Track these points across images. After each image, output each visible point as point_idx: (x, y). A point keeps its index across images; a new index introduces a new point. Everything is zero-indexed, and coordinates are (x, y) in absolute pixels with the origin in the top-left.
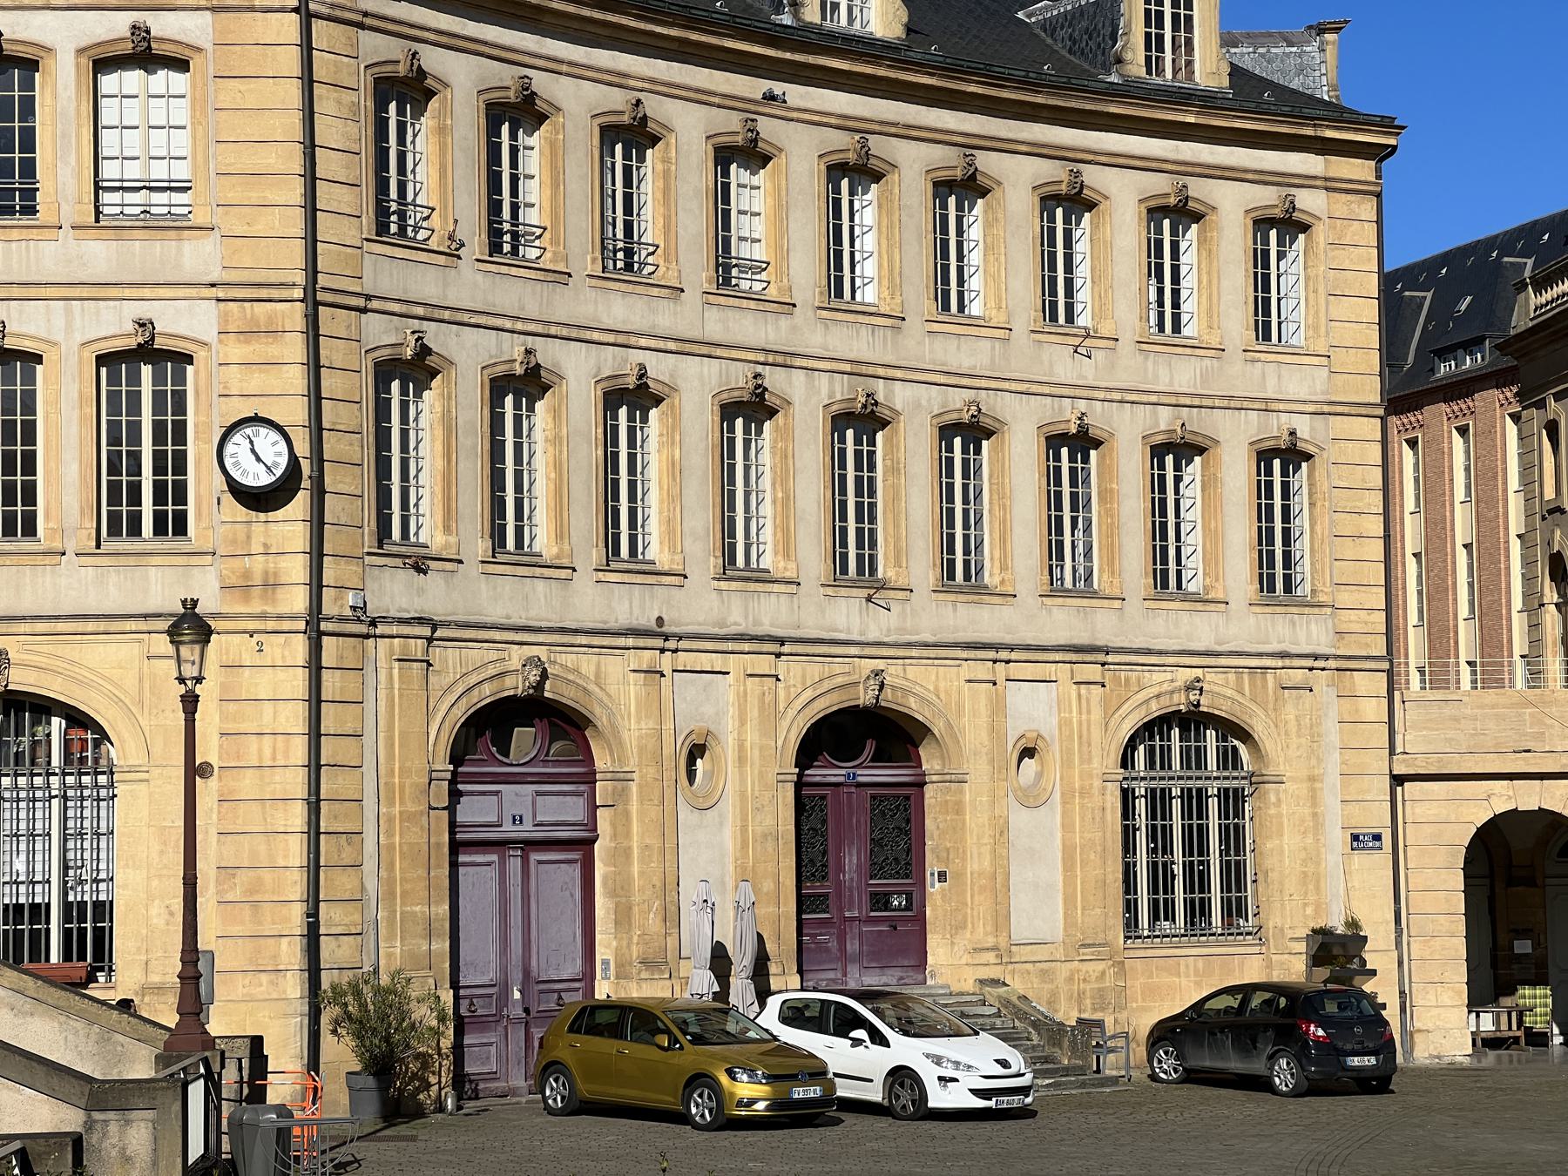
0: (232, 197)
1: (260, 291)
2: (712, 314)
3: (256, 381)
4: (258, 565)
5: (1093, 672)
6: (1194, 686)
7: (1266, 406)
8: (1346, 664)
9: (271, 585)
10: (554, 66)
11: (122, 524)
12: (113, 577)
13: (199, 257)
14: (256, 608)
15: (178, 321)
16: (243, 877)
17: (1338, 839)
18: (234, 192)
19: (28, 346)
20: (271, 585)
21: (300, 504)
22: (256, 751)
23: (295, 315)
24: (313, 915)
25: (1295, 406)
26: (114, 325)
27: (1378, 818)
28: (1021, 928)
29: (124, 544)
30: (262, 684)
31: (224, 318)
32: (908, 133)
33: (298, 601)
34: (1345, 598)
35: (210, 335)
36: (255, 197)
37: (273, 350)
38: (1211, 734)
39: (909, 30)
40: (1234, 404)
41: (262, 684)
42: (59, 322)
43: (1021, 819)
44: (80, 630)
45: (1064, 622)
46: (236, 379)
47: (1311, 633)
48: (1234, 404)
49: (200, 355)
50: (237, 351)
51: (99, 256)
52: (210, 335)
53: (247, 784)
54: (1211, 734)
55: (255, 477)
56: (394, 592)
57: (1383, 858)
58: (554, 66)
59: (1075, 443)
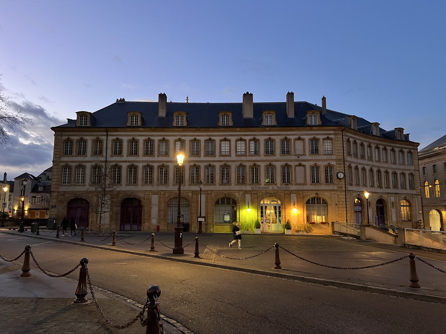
1: (340, 160)
3: (339, 169)
7: (410, 170)
8: (417, 195)
9: (342, 187)
10: (289, 135)
11: (327, 182)
13: (334, 157)
15: (334, 163)
25: (412, 170)
28: (393, 221)
29: (327, 183)
30: (341, 196)
32: (405, 148)
33: (344, 189)
34: (417, 189)
39: (187, 125)
40: (407, 170)
41: (341, 196)
43: (392, 209)
44: (317, 189)
45: (395, 191)
47: (414, 192)
48: (407, 170)
50: (337, 166)
56: (350, 188)
58: (289, 135)
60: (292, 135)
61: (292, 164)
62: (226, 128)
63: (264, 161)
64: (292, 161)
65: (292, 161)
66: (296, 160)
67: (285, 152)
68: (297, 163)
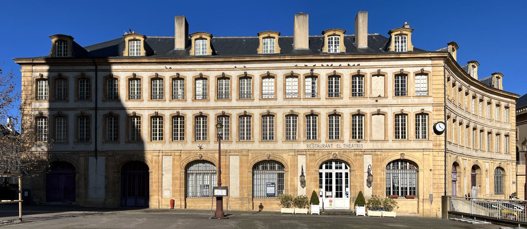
0: (434, 92)
1: (439, 105)
2: (284, 145)
3: (438, 117)
4: (438, 142)
5: (492, 161)
6: (500, 164)
9: (440, 145)
12: (418, 144)
13: (430, 100)
14: (438, 148)
15: (428, 109)
16: (436, 185)
17: (511, 182)
18: (435, 91)
19: (406, 113)
20: (440, 145)
21: (443, 134)
22: (437, 167)
23: (443, 108)
24: (445, 190)
26: (418, 110)
27: (515, 180)
31: (433, 109)
35: (431, 111)
36: (438, 92)
37: (440, 113)
38: (408, 164)
42: (411, 109)
46: (435, 117)
49: (430, 114)
50: (435, 113)
51: (416, 101)
52: (431, 111)
53: (437, 172)
54: (408, 164)
55: (439, 129)
57: (515, 185)
59: (489, 133)
60: (368, 67)
61: (367, 111)
62: (270, 58)
63: (326, 107)
64: (367, 106)
65: (367, 106)
66: (373, 106)
67: (357, 91)
68: (375, 110)
